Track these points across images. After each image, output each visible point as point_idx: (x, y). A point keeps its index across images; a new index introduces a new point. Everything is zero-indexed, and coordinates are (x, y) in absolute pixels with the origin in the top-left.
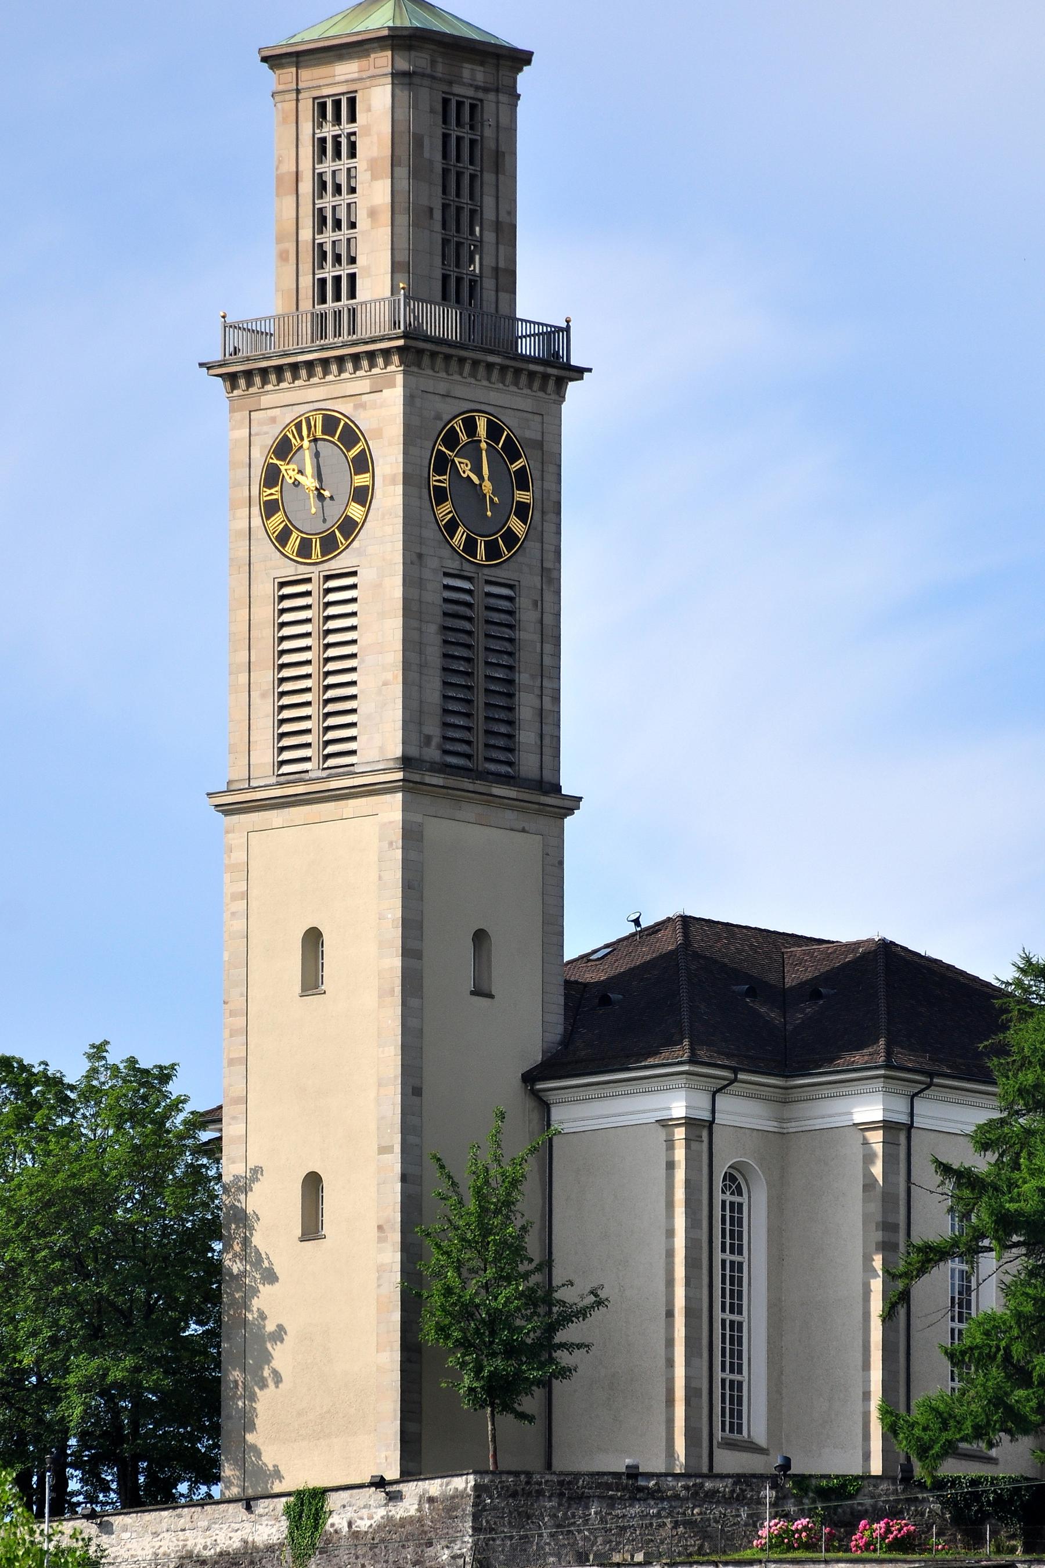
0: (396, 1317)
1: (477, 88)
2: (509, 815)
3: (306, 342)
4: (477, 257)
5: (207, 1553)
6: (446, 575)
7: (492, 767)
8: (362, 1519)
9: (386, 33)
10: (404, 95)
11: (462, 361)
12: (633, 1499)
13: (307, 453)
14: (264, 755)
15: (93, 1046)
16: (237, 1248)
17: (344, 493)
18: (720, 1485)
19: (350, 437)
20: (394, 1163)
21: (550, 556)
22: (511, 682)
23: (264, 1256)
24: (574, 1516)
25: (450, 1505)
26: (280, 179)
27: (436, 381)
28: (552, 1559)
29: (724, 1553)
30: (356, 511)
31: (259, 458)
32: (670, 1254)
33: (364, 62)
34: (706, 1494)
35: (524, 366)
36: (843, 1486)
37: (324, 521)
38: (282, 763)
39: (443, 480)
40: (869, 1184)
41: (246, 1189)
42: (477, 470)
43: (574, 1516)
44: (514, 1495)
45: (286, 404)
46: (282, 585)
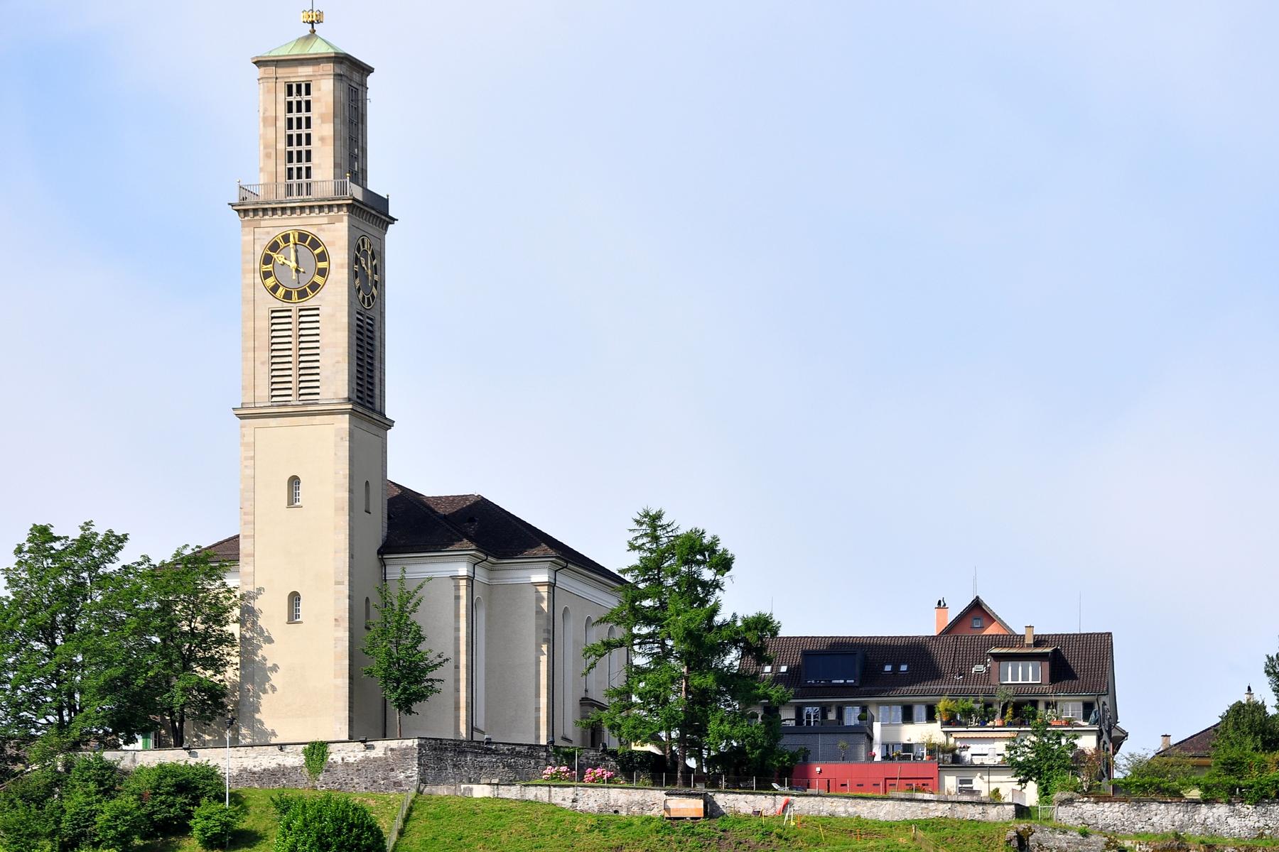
0: (347, 662)
10: (338, 84)
14: (263, 391)
17: (312, 270)
19: (315, 244)
25: (405, 753)
26: (265, 120)
30: (318, 279)
31: (260, 251)
32: (457, 639)
33: (316, 68)
40: (539, 611)
41: (254, 598)
45: (273, 227)
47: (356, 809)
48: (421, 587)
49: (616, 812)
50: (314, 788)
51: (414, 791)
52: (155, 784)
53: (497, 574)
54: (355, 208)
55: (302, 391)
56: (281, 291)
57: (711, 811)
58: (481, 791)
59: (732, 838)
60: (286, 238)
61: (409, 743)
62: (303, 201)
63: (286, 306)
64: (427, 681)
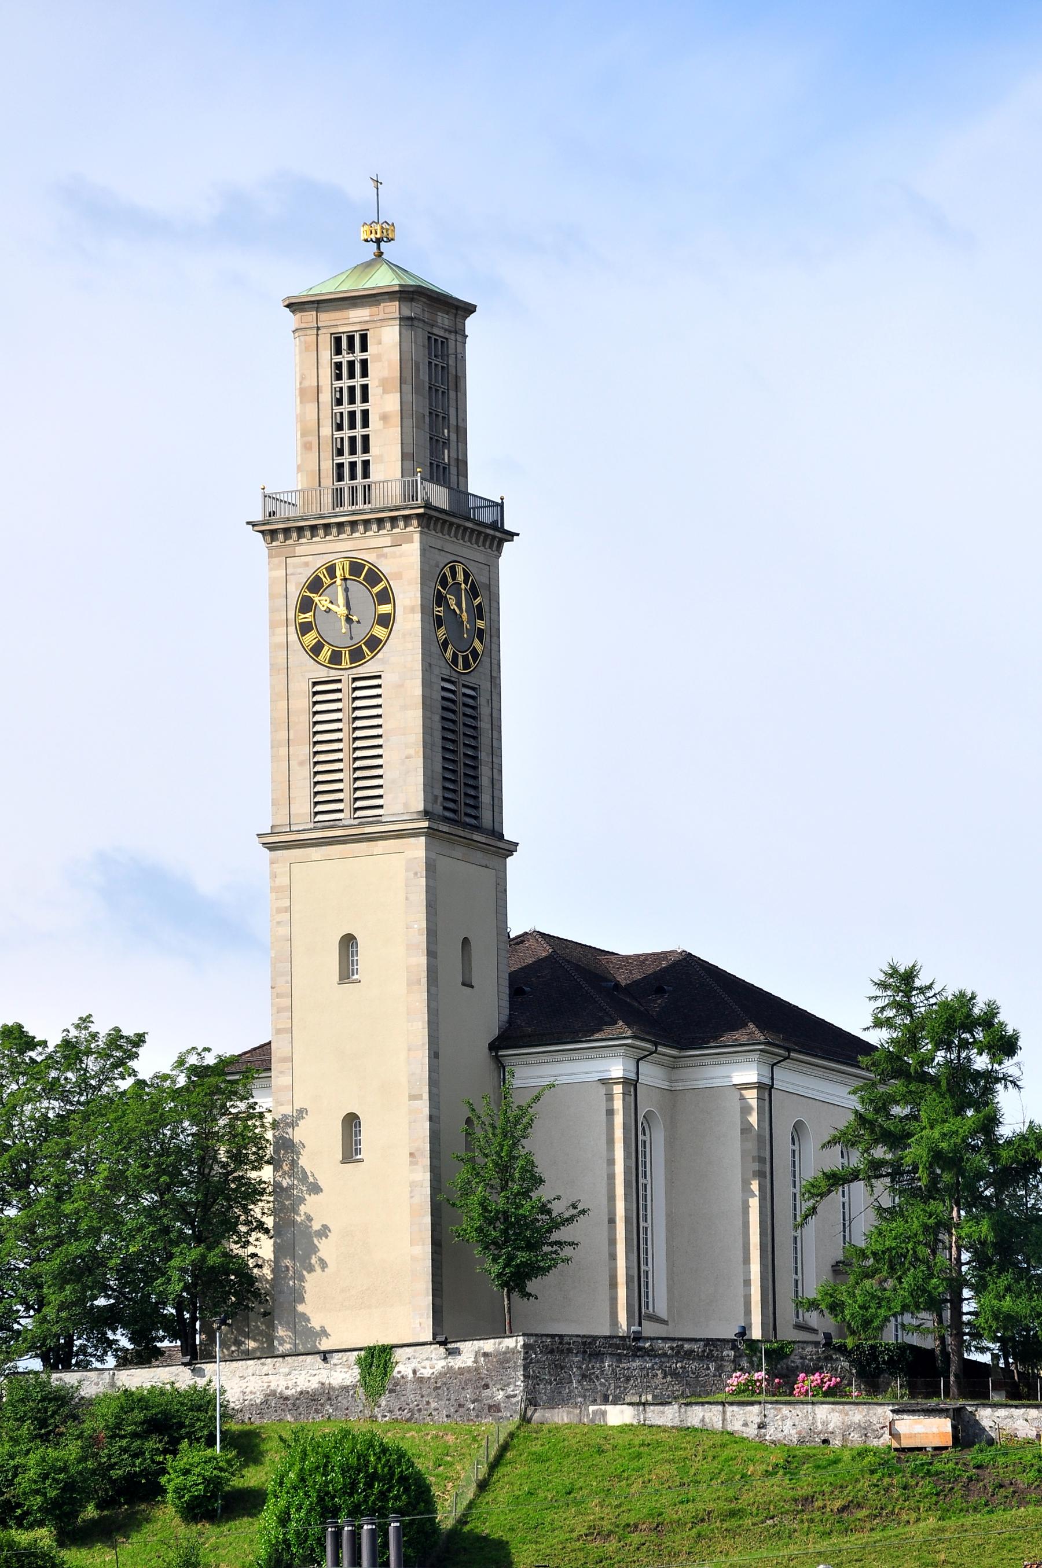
0: (428, 1220)
1: (446, 330)
2: (479, 854)
3: (327, 509)
4: (446, 451)
5: (288, 1393)
6: (443, 679)
7: (468, 820)
8: (425, 1368)
9: (397, 289)
10: (407, 333)
11: (452, 524)
12: (635, 1356)
13: (340, 588)
14: (302, 807)
15: (80, 1019)
16: (286, 1168)
17: (369, 618)
18: (694, 1346)
19: (374, 577)
20: (423, 1107)
21: (495, 667)
22: (475, 758)
23: (309, 1174)
24: (593, 1368)
25: (504, 1359)
26: (303, 392)
27: (438, 540)
28: (579, 1399)
29: (700, 1396)
30: (380, 632)
31: (295, 593)
32: (611, 1177)
33: (375, 309)
34: (686, 1352)
35: (483, 530)
36: (782, 1348)
37: (351, 638)
38: (316, 813)
39: (439, 611)
40: (746, 1128)
41: (293, 1125)
42: (459, 604)
43: (593, 1368)
44: (552, 1352)
45: (313, 555)
46: (315, 684)
47: (385, 1450)
48: (537, 1098)
49: (825, 1441)
50: (373, 1418)
51: (517, 1418)
52: (112, 1421)
53: (684, 1073)
54: (430, 519)
55: (359, 804)
56: (326, 653)
57: (967, 1432)
58: (618, 1415)
59: (989, 1479)
60: (331, 570)
61: (510, 1343)
62: (372, 511)
63: (334, 674)
64: (552, 1244)
